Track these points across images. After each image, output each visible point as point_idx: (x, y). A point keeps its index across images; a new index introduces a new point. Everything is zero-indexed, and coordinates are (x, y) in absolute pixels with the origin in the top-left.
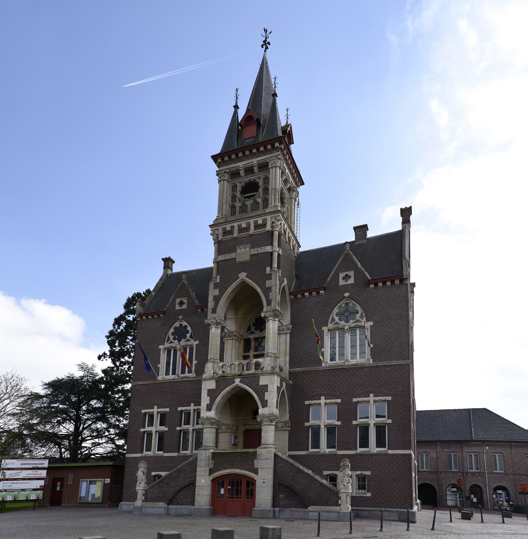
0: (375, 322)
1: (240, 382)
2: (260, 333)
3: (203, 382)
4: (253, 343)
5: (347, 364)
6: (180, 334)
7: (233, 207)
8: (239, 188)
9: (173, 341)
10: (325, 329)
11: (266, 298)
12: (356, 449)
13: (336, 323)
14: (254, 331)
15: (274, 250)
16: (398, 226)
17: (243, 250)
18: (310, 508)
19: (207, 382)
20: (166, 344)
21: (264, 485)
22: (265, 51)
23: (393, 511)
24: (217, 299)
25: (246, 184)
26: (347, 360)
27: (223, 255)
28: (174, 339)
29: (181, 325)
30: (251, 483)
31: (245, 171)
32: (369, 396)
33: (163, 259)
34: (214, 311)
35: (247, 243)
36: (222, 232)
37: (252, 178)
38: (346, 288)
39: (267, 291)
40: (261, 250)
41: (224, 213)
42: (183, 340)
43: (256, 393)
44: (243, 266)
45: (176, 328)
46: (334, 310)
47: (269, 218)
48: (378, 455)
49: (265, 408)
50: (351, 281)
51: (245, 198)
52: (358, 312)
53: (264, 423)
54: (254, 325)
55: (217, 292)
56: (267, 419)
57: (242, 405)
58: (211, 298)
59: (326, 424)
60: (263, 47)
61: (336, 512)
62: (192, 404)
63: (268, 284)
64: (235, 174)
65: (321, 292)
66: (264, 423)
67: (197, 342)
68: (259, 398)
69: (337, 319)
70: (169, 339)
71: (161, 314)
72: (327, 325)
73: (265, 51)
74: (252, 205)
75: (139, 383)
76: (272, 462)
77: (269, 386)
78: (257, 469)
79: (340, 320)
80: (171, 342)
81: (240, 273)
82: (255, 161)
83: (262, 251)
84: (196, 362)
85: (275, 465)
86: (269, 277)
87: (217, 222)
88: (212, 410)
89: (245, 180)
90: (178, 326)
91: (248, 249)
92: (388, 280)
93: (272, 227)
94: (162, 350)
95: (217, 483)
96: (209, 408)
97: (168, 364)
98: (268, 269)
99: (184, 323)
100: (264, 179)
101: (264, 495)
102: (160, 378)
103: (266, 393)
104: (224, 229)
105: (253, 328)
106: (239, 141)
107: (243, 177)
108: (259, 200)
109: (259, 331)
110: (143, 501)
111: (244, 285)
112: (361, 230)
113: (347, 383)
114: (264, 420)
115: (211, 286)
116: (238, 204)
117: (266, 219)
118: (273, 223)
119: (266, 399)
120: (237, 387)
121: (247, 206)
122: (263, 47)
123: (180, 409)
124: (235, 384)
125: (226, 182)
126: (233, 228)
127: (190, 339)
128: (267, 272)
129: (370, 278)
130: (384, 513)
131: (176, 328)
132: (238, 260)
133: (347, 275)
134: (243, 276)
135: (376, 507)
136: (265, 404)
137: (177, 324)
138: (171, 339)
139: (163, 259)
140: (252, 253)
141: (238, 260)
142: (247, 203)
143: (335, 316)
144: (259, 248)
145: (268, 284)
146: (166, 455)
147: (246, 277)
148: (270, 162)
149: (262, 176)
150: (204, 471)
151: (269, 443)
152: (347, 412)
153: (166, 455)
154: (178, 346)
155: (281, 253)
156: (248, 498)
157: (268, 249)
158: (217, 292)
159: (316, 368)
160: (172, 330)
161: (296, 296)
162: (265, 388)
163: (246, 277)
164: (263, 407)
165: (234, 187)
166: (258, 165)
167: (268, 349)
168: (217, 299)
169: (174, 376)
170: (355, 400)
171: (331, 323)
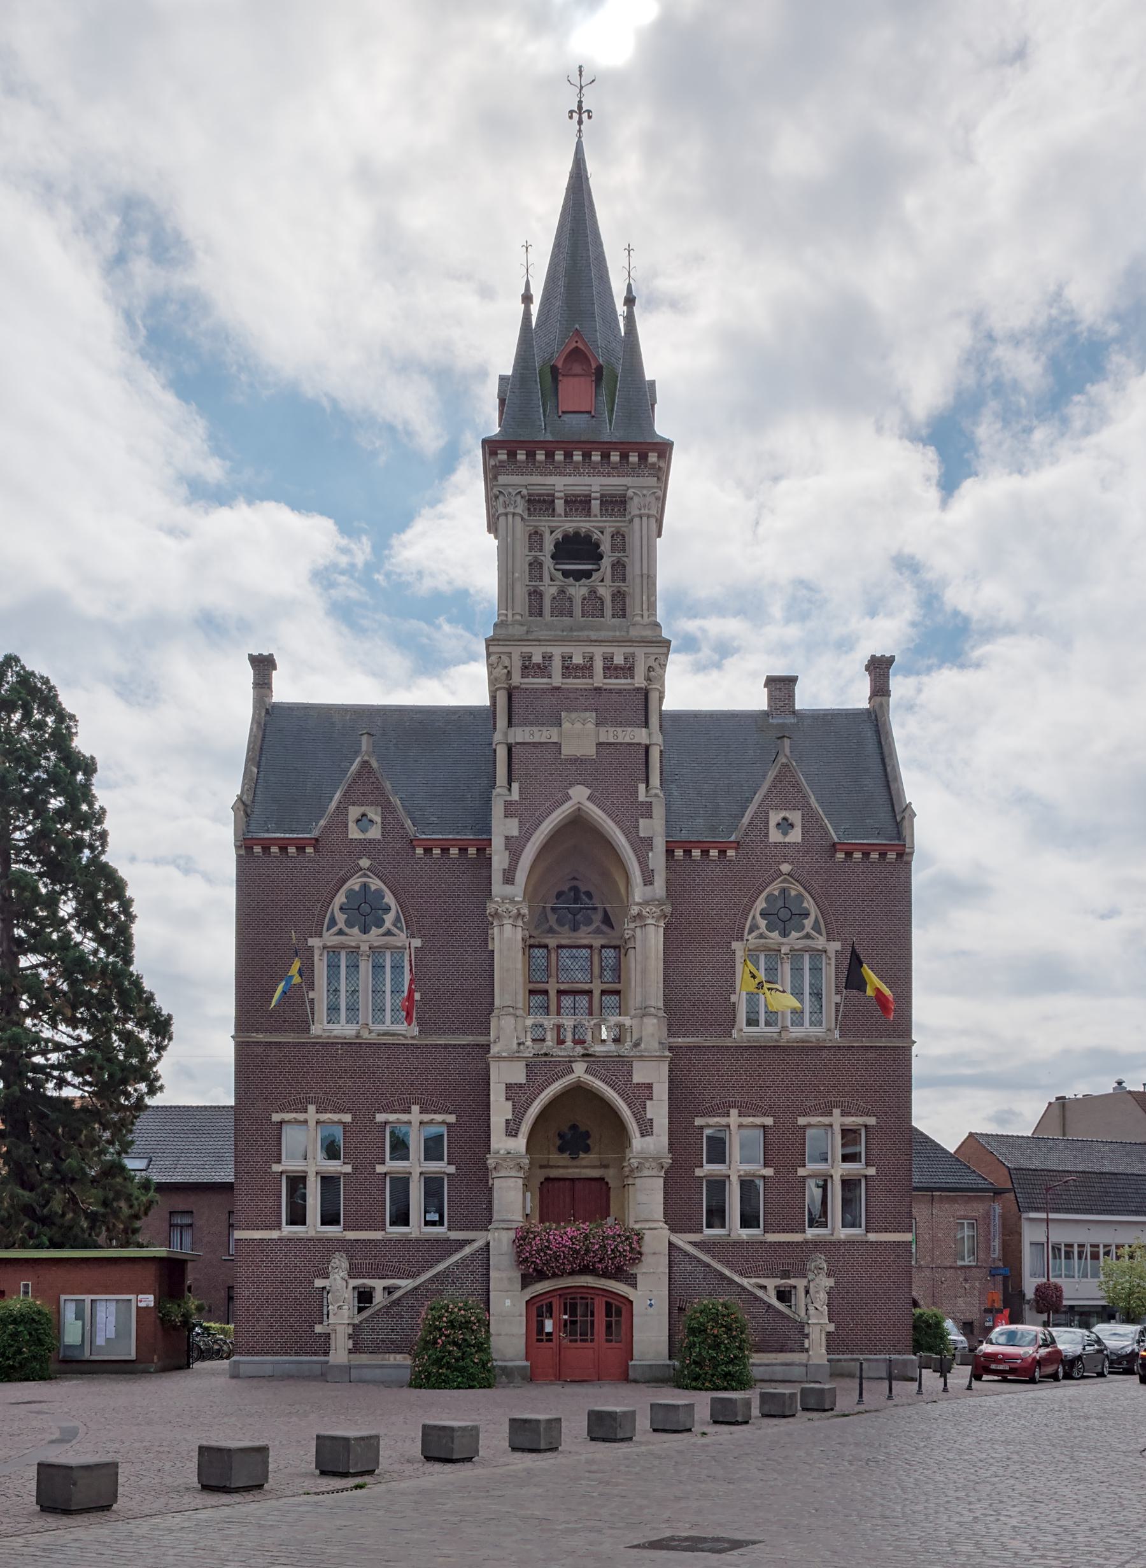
2: (573, 934)
7: (536, 595)
9: (347, 930)
11: (640, 863)
15: (654, 741)
16: (859, 697)
17: (578, 725)
20: (326, 934)
21: (651, 1310)
23: (877, 1360)
24: (514, 847)
25: (566, 537)
26: (784, 1028)
27: (527, 729)
28: (349, 923)
29: (365, 886)
30: (619, 1311)
31: (566, 502)
32: (831, 1114)
34: (509, 879)
35: (586, 710)
36: (520, 664)
38: (365, 848)
41: (518, 610)
42: (374, 931)
43: (625, 1100)
44: (579, 769)
47: (640, 652)
48: (849, 1243)
49: (647, 1138)
51: (566, 574)
53: (646, 1173)
55: (512, 827)
56: (654, 1164)
57: (578, 1126)
58: (498, 843)
59: (742, 1173)
60: (571, 117)
61: (800, 1365)
62: (415, 1108)
63: (645, 827)
64: (540, 503)
66: (646, 1173)
68: (634, 1114)
70: (333, 922)
71: (309, 845)
74: (584, 599)
75: (260, 1037)
76: (665, 1261)
77: (655, 1086)
79: (770, 928)
80: (341, 932)
81: (571, 785)
82: (595, 484)
83: (627, 740)
86: (647, 810)
87: (502, 632)
88: (520, 1135)
89: (567, 525)
90: (357, 888)
91: (591, 726)
92: (875, 850)
93: (648, 679)
94: (317, 953)
95: (538, 1309)
96: (512, 1130)
99: (375, 884)
101: (651, 1334)
102: (316, 1029)
103: (648, 1103)
104: (608, 658)
108: (605, 592)
111: (578, 823)
112: (781, 687)
113: (784, 1077)
114: (647, 1165)
115: (498, 809)
117: (633, 655)
121: (570, 599)
122: (571, 117)
123: (380, 1117)
124: (573, 1076)
125: (518, 519)
126: (547, 657)
127: (395, 931)
128: (642, 797)
129: (836, 840)
130: (865, 1365)
131: (350, 894)
132: (567, 751)
133: (785, 819)
134: (579, 794)
135: (843, 1353)
137: (354, 883)
138: (341, 924)
141: (567, 751)
142: (571, 591)
143: (758, 917)
144: (619, 730)
145: (645, 827)
148: (636, 499)
150: (510, 1279)
152: (783, 1148)
156: (611, 1341)
158: (512, 827)
159: (719, 1042)
160: (340, 899)
165: (535, 538)
166: (602, 496)
168: (514, 847)
170: (802, 1121)
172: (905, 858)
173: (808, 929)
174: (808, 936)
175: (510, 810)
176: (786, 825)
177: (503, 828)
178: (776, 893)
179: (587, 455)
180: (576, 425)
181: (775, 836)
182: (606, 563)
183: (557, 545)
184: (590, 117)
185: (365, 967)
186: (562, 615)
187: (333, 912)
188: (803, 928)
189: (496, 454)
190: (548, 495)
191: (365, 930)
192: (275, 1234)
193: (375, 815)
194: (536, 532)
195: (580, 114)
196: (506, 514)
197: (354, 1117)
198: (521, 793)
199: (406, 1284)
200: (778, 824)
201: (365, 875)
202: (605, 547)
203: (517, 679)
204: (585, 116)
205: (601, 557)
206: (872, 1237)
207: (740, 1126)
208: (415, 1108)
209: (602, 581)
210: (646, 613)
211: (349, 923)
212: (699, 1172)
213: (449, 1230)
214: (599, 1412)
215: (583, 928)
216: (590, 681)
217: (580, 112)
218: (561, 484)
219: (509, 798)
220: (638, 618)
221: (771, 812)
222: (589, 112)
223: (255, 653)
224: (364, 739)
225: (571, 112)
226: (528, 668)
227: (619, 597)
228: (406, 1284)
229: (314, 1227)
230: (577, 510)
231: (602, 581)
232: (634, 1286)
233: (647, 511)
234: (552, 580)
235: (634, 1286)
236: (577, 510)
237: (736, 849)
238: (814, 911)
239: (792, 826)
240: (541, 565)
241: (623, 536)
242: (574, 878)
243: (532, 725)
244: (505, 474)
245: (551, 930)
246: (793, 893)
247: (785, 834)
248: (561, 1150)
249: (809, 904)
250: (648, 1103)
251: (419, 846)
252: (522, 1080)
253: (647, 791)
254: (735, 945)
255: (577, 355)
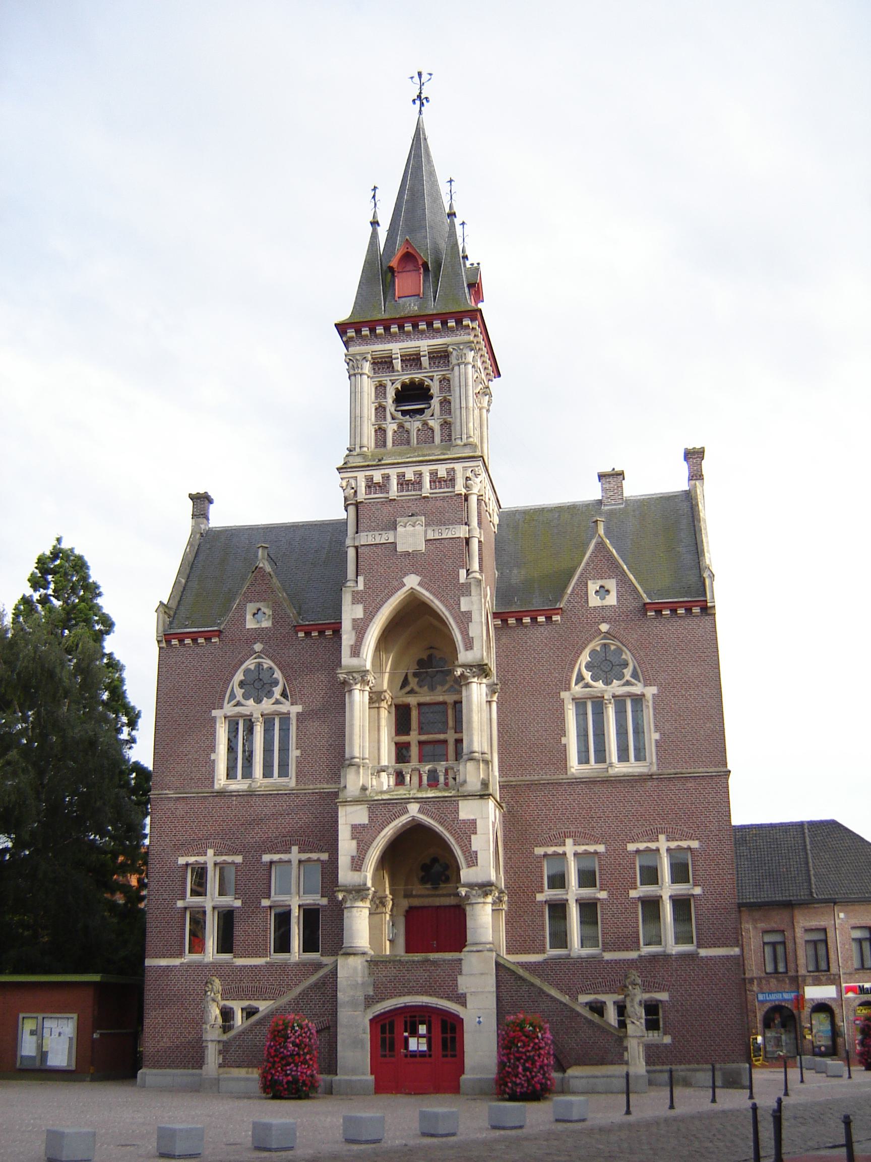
0: (660, 685)
1: (420, 811)
3: (340, 808)
4: (414, 714)
5: (611, 772)
6: (258, 686)
8: (391, 394)
9: (243, 701)
10: (564, 695)
11: (462, 633)
12: (543, 951)
13: (587, 686)
14: (417, 688)
16: (676, 480)
18: (571, 1072)
19: (350, 809)
22: (420, 93)
24: (360, 628)
25: (404, 385)
26: (611, 765)
28: (246, 697)
29: (259, 665)
33: (191, 497)
34: (356, 651)
37: (418, 376)
38: (603, 614)
39: (465, 619)
40: (448, 533)
45: (247, 672)
46: (581, 657)
47: (458, 467)
48: (683, 956)
50: (612, 600)
52: (626, 665)
54: (415, 675)
55: (359, 612)
57: (422, 861)
62: (295, 849)
64: (383, 363)
65: (555, 618)
67: (298, 708)
69: (587, 675)
70: (233, 696)
71: (215, 636)
72: (568, 688)
73: (420, 93)
74: (419, 430)
76: (492, 980)
77: (478, 822)
78: (464, 996)
79: (594, 679)
80: (238, 704)
81: (406, 574)
82: (424, 345)
83: (450, 536)
84: (297, 753)
85: (498, 987)
86: (465, 590)
89: (404, 377)
90: (252, 667)
93: (467, 487)
96: (357, 864)
97: (231, 749)
98: (463, 573)
99: (267, 663)
100: (440, 382)
103: (473, 837)
104: (370, 479)
105: (413, 682)
106: (389, 298)
107: (398, 371)
108: (434, 424)
109: (426, 688)
110: (220, 1066)
115: (347, 598)
116: (391, 428)
117: (453, 469)
118: (468, 479)
119: (474, 849)
120: (414, 819)
121: (408, 432)
125: (365, 377)
128: (462, 580)
131: (247, 672)
136: (472, 860)
137: (250, 664)
139: (191, 497)
140: (430, 536)
142: (407, 425)
146: (240, 962)
147: (419, 584)
148: (455, 353)
149: (437, 376)
151: (483, 940)
153: (240, 962)
154: (257, 715)
155: (482, 539)
156: (446, 1056)
157: (461, 532)
158: (359, 612)
160: (239, 676)
161: (505, 621)
162: (471, 827)
163: (419, 584)
164: (469, 866)
165: (381, 388)
167: (471, 742)
169: (248, 781)
171: (576, 684)
172: (709, 611)
173: (628, 677)
174: (628, 683)
175: (357, 598)
176: (603, 591)
177: (351, 612)
178: (598, 648)
179: (401, 327)
180: (412, 307)
181: (594, 601)
182: (435, 402)
183: (398, 393)
184: (428, 101)
185: (259, 730)
186: (401, 444)
187: (580, 669)
188: (623, 676)
189: (346, 333)
190: (387, 357)
191: (258, 701)
192: (176, 962)
193: (611, 584)
194: (381, 385)
195: (420, 100)
196: (459, 365)
197: (244, 858)
198: (365, 584)
199: (264, 1006)
200: (597, 592)
201: (259, 657)
202: (435, 389)
203: (362, 495)
204: (424, 101)
205: (431, 397)
206: (703, 952)
207: (576, 854)
208: (295, 849)
209: (432, 415)
210: (464, 437)
211: (246, 697)
212: (540, 897)
213: (322, 955)
214: (163, 1128)
215: (439, 688)
216: (419, 493)
217: (420, 99)
218: (396, 348)
219: (356, 589)
220: (459, 442)
221: (590, 583)
222: (426, 98)
223: (194, 492)
224: (260, 551)
225: (414, 101)
226: (371, 485)
227: (446, 425)
228: (264, 1006)
229: (211, 952)
230: (411, 366)
231: (432, 415)
232: (464, 1004)
233: (360, 371)
234: (393, 418)
235: (464, 1004)
236: (411, 366)
237: (219, 636)
238: (281, 681)
239: (608, 591)
240: (384, 408)
241: (449, 381)
242: (431, 648)
243: (374, 530)
244: (354, 346)
245: (412, 692)
246: (265, 666)
247: (603, 598)
248: (423, 881)
249: (627, 656)
250: (473, 837)
251: (301, 631)
252: (365, 820)
253: (468, 575)
254: (563, 695)
255: (409, 257)
